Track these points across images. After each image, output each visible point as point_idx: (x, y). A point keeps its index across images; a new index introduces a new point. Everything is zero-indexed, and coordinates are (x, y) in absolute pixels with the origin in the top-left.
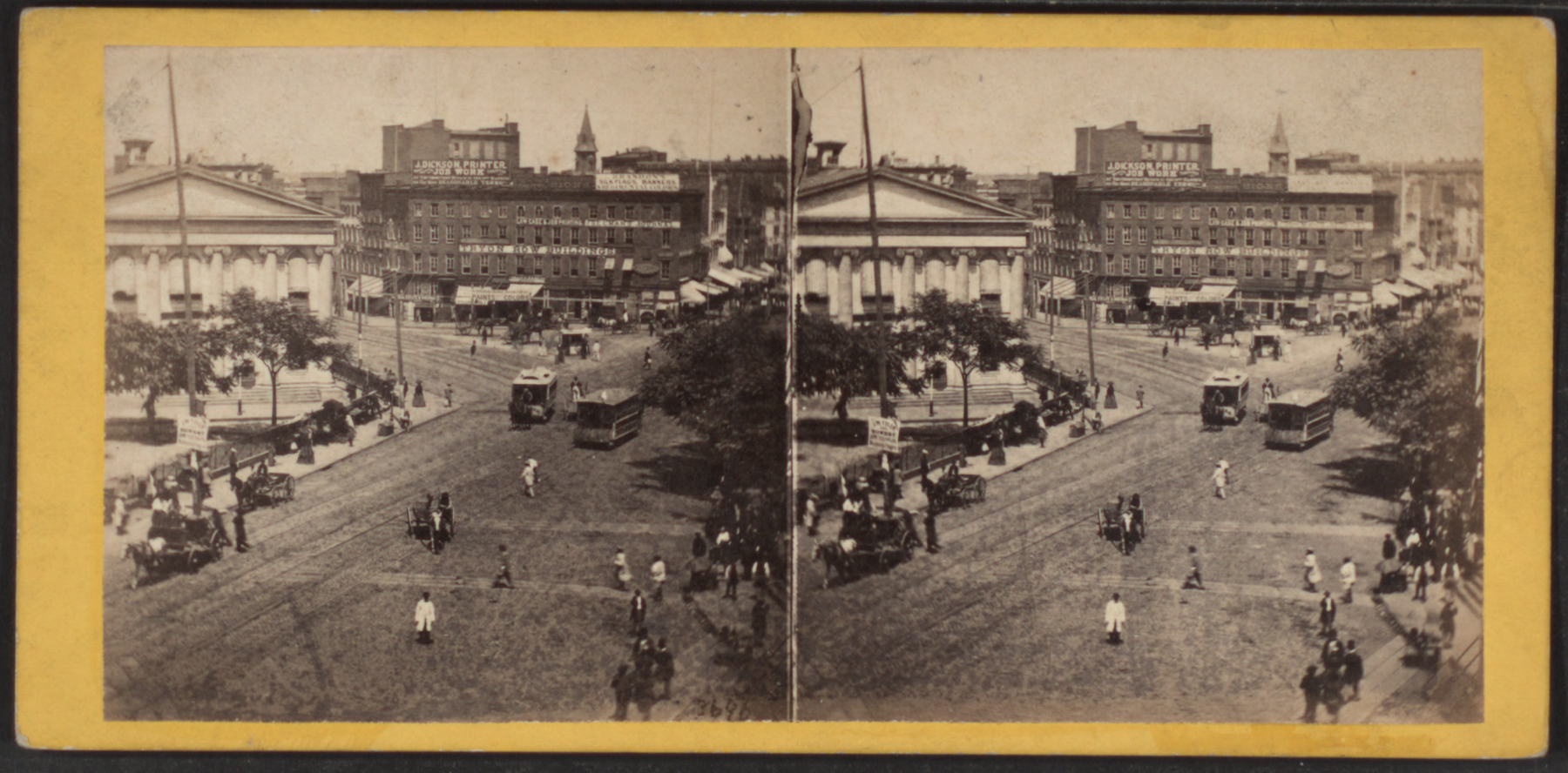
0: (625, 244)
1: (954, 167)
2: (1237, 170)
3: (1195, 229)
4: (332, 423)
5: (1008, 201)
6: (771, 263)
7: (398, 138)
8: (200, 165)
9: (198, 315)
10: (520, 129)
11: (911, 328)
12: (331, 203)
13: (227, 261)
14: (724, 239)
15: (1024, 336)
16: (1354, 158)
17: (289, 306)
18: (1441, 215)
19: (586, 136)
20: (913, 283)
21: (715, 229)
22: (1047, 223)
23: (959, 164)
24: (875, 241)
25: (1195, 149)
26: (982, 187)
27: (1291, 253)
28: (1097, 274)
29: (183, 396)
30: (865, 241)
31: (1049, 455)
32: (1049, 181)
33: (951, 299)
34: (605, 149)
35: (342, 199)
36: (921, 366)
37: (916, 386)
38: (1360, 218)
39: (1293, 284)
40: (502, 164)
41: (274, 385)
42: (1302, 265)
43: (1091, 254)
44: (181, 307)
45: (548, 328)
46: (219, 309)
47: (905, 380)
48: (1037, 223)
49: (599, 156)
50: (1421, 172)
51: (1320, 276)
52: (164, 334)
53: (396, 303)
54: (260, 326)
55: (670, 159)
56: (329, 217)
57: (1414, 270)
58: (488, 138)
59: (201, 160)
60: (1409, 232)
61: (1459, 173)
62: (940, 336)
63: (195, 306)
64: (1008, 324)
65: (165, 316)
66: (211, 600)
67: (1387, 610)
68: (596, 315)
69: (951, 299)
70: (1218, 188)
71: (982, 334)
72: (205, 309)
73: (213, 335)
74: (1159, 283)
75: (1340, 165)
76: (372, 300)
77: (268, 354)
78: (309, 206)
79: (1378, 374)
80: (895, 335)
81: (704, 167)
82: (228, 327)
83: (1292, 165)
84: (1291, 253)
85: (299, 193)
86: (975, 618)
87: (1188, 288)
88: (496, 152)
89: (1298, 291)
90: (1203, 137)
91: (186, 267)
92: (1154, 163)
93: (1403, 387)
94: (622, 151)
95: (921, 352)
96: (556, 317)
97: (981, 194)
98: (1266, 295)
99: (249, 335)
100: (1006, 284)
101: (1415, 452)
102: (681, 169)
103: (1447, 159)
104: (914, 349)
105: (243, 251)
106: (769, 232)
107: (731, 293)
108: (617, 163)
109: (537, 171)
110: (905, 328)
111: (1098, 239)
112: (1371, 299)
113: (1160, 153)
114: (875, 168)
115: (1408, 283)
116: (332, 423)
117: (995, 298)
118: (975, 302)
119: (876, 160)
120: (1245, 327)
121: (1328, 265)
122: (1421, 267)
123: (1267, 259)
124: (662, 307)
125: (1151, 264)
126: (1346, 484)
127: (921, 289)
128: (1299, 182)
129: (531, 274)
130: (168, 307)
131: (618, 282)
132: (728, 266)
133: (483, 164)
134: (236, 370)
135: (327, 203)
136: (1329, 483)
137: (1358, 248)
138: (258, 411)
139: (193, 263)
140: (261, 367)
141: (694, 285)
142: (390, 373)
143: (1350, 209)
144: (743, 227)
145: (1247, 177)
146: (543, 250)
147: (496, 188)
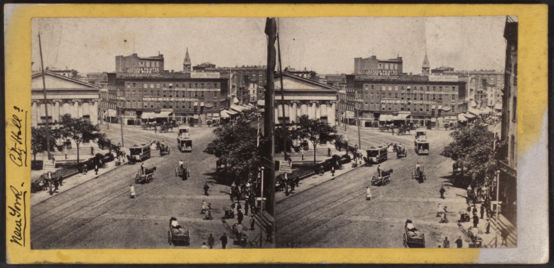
0: (201, 97)
1: (311, 72)
2: (173, 71)
4: (96, 162)
5: (330, 84)
6: (252, 103)
7: (120, 59)
8: (51, 71)
9: (51, 124)
10: (164, 57)
11: (296, 129)
12: (98, 83)
14: (236, 95)
15: (336, 132)
16: (452, 69)
17: (83, 120)
18: (482, 90)
19: (187, 59)
20: (59, 111)
21: (233, 92)
22: (105, 89)
24: (283, 97)
25: (396, 66)
26: (321, 79)
27: (192, 100)
28: (362, 110)
29: (46, 153)
30: (41, 97)
31: (108, 172)
32: (345, 77)
33: (310, 118)
34: (433, 67)
35: (340, 84)
36: (299, 142)
37: (297, 149)
38: (216, 87)
39: (431, 113)
40: (158, 69)
41: (315, 149)
42: (196, 104)
43: (122, 101)
44: (45, 121)
45: (175, 127)
46: (58, 122)
47: (293, 147)
48: (341, 91)
49: (430, 69)
50: (237, 71)
51: (202, 108)
52: (39, 131)
53: (121, 119)
54: (73, 127)
55: (217, 67)
56: (97, 88)
57: (473, 109)
58: (157, 60)
59: (51, 69)
60: (232, 93)
61: (489, 75)
62: (306, 132)
63: (287, 122)
64: (330, 128)
65: (39, 124)
66: (56, 225)
67: (227, 225)
68: (192, 122)
69: (310, 118)
70: (166, 77)
71: (321, 131)
72: (291, 122)
73: (56, 131)
74: (384, 113)
75: (447, 72)
76: (113, 118)
77: (75, 138)
78: (89, 84)
79: (223, 142)
80: (289, 131)
81: (228, 70)
82: (61, 128)
83: (192, 69)
85: (86, 80)
86: (318, 231)
87: (394, 115)
88: (394, 67)
89: (433, 115)
90: (399, 62)
91: (46, 107)
93: (232, 146)
94: (438, 67)
95: (299, 137)
96: (415, 126)
97: (321, 82)
98: (420, 117)
99: (69, 131)
100: (329, 112)
101: (237, 169)
102: (220, 70)
103: (246, 66)
104: (297, 136)
105: (66, 101)
106: (251, 92)
107: (239, 114)
108: (197, 68)
109: (170, 71)
110: (293, 128)
111: (124, 95)
112: (220, 116)
113: (384, 67)
114: (45, 71)
116: (96, 162)
117: (325, 118)
119: (45, 68)
120: (413, 128)
121: (443, 107)
122: (475, 107)
123: (183, 102)
124: (214, 119)
125: (381, 106)
127: (299, 115)
128: (433, 78)
129: (168, 108)
130: (40, 121)
131: (199, 110)
132: (237, 104)
133: (151, 69)
134: (301, 144)
135: (96, 83)
136: (208, 180)
137: (453, 101)
138: (72, 157)
139: (286, 106)
140: (73, 143)
141: (225, 111)
142: (119, 144)
143: (212, 84)
144: (242, 90)
145: (176, 73)
146: (172, 99)
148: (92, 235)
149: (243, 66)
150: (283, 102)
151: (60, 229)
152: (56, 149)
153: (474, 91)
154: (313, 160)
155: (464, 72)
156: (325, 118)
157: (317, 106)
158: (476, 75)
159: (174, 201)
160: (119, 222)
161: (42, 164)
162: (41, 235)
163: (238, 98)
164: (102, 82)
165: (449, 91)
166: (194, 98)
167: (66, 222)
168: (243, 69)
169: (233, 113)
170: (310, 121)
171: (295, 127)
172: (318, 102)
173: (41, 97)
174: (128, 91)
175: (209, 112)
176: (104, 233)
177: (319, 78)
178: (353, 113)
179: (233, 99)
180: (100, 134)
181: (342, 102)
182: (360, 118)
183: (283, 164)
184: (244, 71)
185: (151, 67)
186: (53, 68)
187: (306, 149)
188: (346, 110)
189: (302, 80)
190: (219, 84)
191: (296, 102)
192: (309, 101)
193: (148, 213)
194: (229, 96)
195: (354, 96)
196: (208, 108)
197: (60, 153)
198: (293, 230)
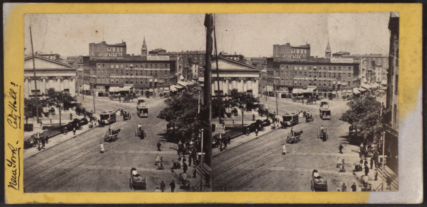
0: (155, 75)
1: (240, 55)
2: (133, 55)
3: (305, 72)
4: (74, 125)
5: (255, 65)
7: (92, 46)
8: (39, 55)
9: (39, 96)
11: (228, 99)
12: (76, 64)
13: (61, 80)
14: (182, 73)
15: (259, 102)
17: (64, 93)
18: (372, 69)
19: (144, 46)
21: (179, 71)
22: (81, 69)
23: (57, 54)
24: (218, 75)
25: (305, 51)
26: (247, 61)
27: (148, 77)
28: (279, 85)
29: (35, 118)
30: (32, 75)
32: (266, 59)
33: (239, 91)
34: (333, 52)
35: (262, 65)
36: (231, 109)
37: (229, 115)
38: (166, 67)
39: (332, 88)
40: (122, 53)
41: (243, 115)
42: (151, 80)
43: (94, 78)
44: (34, 94)
45: (318, 100)
47: (226, 113)
49: (148, 51)
50: (183, 55)
51: (156, 83)
52: (30, 101)
53: (93, 92)
54: (56, 98)
55: (167, 52)
56: (75, 68)
58: (121, 46)
59: (39, 53)
61: (377, 58)
62: (236, 102)
63: (221, 94)
64: (254, 98)
65: (30, 96)
66: (43, 174)
67: (175, 174)
68: (148, 94)
69: (239, 91)
70: (128, 59)
71: (247, 101)
72: (41, 94)
73: (43, 101)
76: (87, 91)
77: (58, 106)
78: (69, 65)
79: (172, 109)
80: (223, 101)
81: (176, 54)
82: (47, 99)
83: (148, 53)
84: (331, 79)
85: (67, 62)
86: (245, 178)
87: (120, 87)
88: (304, 52)
89: (334, 89)
90: (308, 48)
91: (36, 83)
92: (294, 55)
93: (179, 113)
95: (230, 106)
96: (320, 97)
97: (247, 63)
98: (324, 91)
101: (182, 131)
102: (169, 54)
104: (229, 105)
106: (194, 71)
107: (184, 88)
109: (131, 55)
110: (226, 99)
111: (95, 74)
112: (170, 89)
114: (35, 55)
115: (363, 87)
116: (74, 125)
117: (251, 91)
118: (62, 91)
119: (34, 52)
120: (318, 99)
122: (366, 83)
123: (141, 79)
124: (165, 92)
125: (293, 82)
126: (347, 142)
127: (231, 88)
128: (333, 60)
129: (129, 83)
130: (31, 94)
131: (153, 85)
132: (183, 80)
133: (116, 54)
134: (232, 111)
135: (74, 64)
136: (160, 139)
137: (349, 78)
138: (56, 122)
139: (220, 82)
140: (57, 110)
141: (174, 86)
142: (92, 111)
143: (164, 65)
144: (187, 70)
145: (136, 56)
146: (133, 77)
147: (304, 62)
148: (71, 181)
149: (188, 51)
150: (218, 79)
151: (47, 177)
152: (43, 115)
153: (365, 70)
154: (241, 123)
155: (358, 56)
156: (251, 91)
157: (245, 82)
158: (367, 58)
159: (134, 155)
160: (91, 171)
161: (33, 127)
162: (32, 181)
163: (184, 76)
164: (78, 63)
165: (346, 70)
166: (150, 75)
167: (51, 171)
168: (187, 53)
169: (180, 87)
170: (239, 93)
171: (227, 98)
172: (245, 79)
173: (32, 75)
174: (99, 70)
175: (161, 87)
176: (80, 180)
177: (246, 60)
178: (272, 87)
179: (179, 76)
180: (77, 104)
181: (264, 79)
182: (277, 91)
183: (218, 127)
184: (188, 55)
185: (116, 52)
186: (41, 52)
187: (236, 115)
188: (267, 85)
189: (233, 62)
190: (169, 65)
191: (228, 79)
192: (238, 78)
193: (114, 165)
194: (177, 74)
195: (273, 74)
196: (160, 84)
197: (46, 118)
198: (226, 177)
